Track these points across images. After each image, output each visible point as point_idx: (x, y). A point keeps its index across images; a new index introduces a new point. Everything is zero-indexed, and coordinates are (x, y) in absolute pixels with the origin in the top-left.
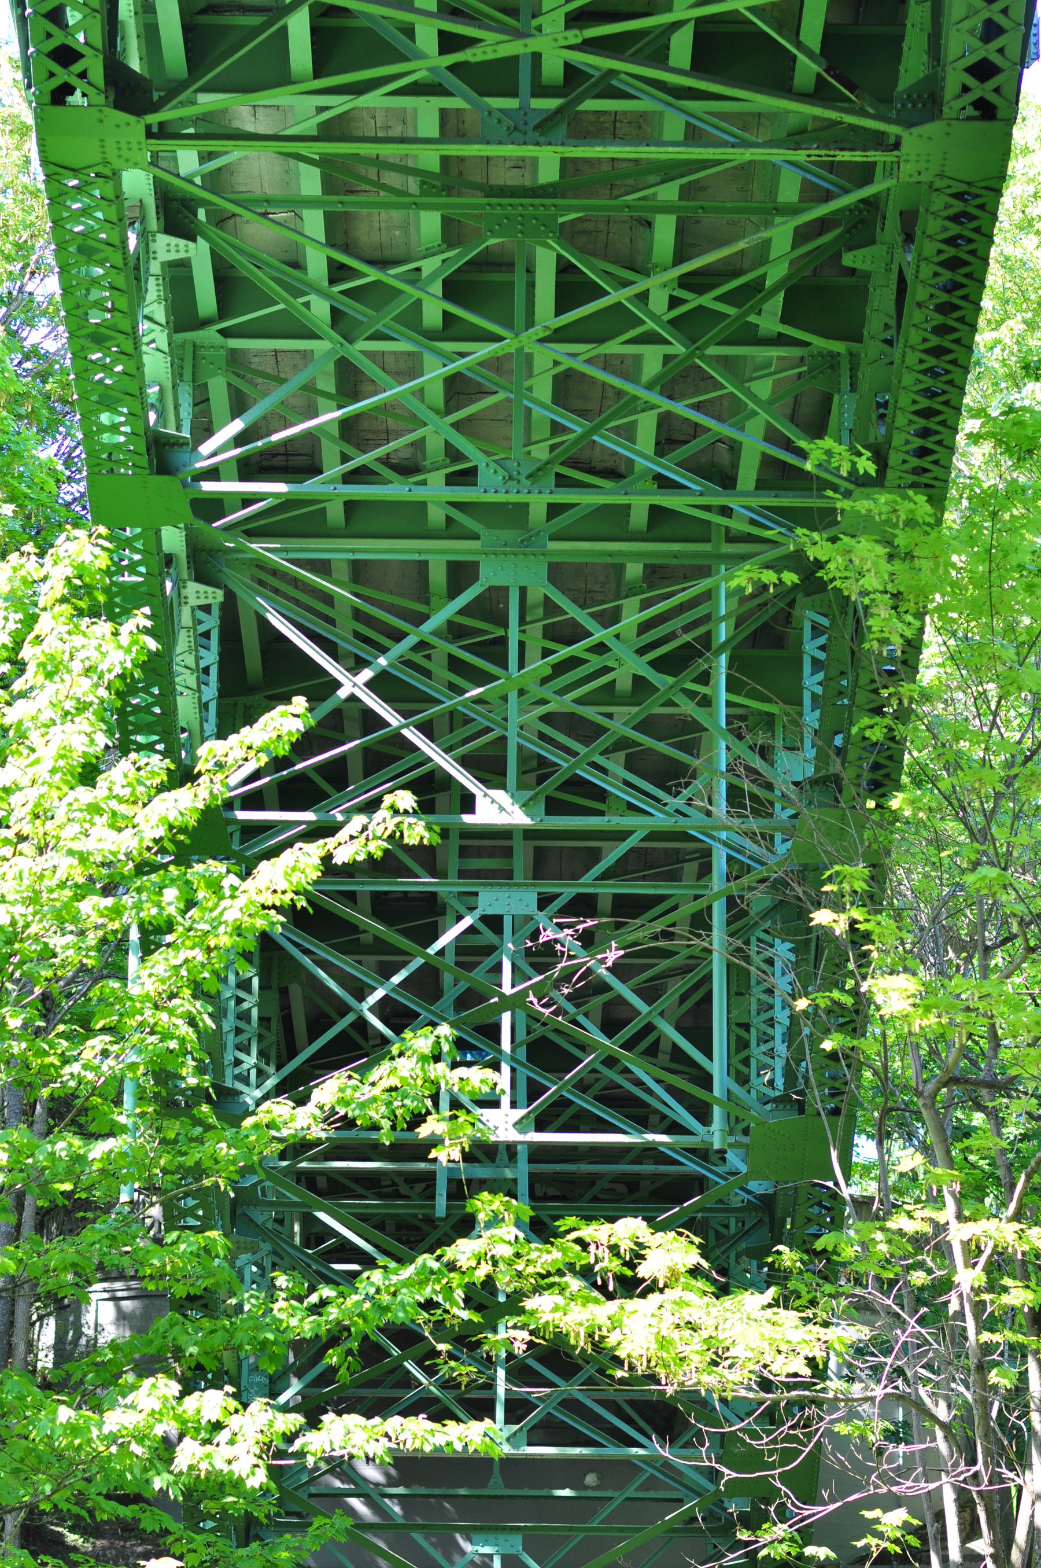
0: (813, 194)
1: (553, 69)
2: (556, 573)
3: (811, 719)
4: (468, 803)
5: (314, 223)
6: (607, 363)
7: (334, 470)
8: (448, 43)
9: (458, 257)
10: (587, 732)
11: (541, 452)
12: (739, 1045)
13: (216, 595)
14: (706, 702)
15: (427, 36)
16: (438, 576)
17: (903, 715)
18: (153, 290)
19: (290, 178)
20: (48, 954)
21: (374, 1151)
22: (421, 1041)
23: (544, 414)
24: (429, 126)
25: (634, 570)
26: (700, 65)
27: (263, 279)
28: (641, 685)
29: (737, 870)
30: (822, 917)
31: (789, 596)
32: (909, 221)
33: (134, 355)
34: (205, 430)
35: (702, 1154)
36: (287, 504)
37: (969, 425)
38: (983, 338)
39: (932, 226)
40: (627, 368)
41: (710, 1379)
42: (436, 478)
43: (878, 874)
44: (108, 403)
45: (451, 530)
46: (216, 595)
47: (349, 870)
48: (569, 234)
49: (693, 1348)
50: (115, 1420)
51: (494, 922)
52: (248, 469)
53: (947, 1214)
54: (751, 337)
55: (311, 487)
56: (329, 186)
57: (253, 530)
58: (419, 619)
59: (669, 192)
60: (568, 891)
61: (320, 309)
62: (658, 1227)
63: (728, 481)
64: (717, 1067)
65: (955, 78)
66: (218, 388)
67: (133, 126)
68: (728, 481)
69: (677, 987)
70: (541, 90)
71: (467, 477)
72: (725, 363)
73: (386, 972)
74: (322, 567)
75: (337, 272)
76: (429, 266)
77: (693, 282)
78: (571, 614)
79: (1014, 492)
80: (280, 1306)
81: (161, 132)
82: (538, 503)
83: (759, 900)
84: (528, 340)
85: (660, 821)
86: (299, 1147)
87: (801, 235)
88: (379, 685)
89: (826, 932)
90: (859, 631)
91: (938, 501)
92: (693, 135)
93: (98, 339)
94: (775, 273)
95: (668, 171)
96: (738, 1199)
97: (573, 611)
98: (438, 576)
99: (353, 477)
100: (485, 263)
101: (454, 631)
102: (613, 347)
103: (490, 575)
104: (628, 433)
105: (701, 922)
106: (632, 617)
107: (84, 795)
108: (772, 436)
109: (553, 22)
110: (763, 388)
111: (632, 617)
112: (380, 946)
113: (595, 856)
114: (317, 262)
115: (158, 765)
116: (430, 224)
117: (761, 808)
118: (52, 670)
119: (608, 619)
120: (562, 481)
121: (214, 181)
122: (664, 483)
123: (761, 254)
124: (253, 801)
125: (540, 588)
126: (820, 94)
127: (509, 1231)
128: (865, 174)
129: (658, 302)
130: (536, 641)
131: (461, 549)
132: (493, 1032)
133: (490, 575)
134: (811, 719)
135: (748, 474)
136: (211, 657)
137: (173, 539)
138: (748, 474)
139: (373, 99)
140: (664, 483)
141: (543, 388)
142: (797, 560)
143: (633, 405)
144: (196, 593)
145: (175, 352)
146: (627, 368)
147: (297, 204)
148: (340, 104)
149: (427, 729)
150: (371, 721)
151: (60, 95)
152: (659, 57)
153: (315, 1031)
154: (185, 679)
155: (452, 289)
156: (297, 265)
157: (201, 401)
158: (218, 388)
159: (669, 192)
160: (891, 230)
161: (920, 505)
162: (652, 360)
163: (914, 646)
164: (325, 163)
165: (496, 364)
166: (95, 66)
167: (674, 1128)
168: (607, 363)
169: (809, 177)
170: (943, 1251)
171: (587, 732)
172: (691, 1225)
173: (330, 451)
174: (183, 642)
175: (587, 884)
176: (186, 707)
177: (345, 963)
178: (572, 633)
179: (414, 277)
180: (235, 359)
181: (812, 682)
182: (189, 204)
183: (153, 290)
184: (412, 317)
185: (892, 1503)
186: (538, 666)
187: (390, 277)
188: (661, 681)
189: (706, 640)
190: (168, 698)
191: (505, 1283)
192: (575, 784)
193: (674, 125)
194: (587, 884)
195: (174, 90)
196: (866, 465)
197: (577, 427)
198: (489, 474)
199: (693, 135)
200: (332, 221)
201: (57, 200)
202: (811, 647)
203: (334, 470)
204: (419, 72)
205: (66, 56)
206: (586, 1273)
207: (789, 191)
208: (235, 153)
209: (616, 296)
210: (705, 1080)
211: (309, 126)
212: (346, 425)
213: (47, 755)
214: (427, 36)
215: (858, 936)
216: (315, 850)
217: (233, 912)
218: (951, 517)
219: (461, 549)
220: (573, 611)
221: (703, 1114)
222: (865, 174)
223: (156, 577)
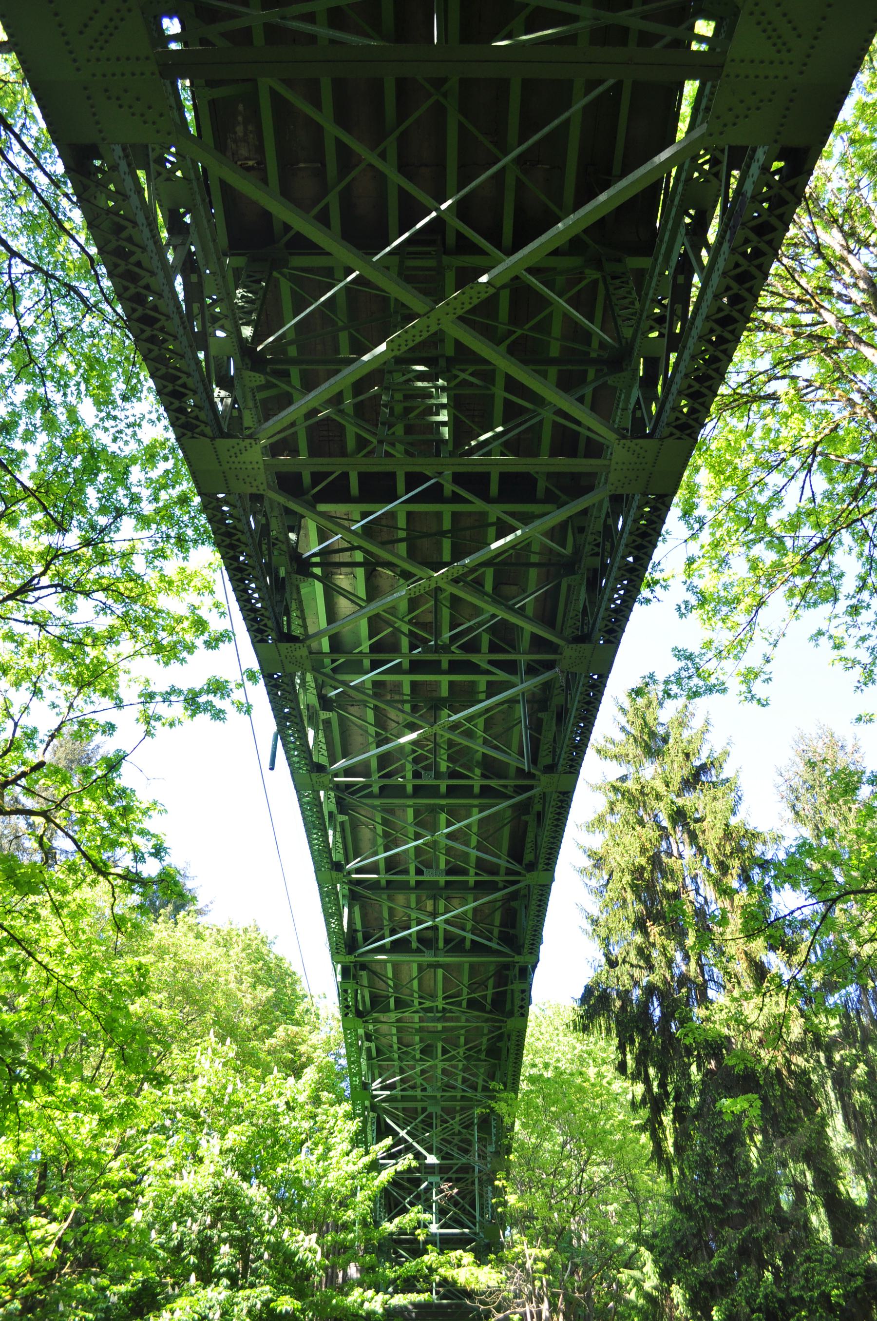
0: (491, 1032)
1: (440, 1007)
2: (443, 1109)
3: (494, 1138)
4: (425, 1158)
5: (395, 1039)
6: (451, 1066)
7: (399, 1088)
8: (420, 1003)
9: (423, 1045)
10: (450, 1143)
11: (439, 1084)
12: (481, 1209)
13: (375, 1115)
14: (473, 1135)
15: (416, 1002)
16: (419, 1110)
17: (511, 1139)
18: (364, 1052)
19: (390, 1030)
20: (339, 1192)
21: (406, 1234)
22: (415, 1209)
23: (440, 1076)
24: (417, 1020)
25: (458, 1108)
26: (468, 1007)
27: (384, 1050)
28: (460, 1133)
29: (480, 1171)
30: (497, 1183)
31: (488, 1115)
32: (509, 1037)
33: (360, 1066)
34: (373, 1080)
35: (475, 1234)
36: (388, 1096)
37: (522, 1078)
38: (524, 1059)
39: (514, 1038)
40: (455, 1067)
41: (477, 1287)
42: (419, 1090)
43: (508, 1174)
44: (355, 1075)
45: (422, 1100)
46: (375, 1115)
47: (401, 1172)
48: (444, 1040)
49: (472, 1279)
50: (350, 1299)
51: (431, 1183)
52: (382, 1089)
53: (525, 1247)
54: (479, 1060)
55: (394, 1092)
56: (398, 1031)
57: (383, 1101)
58: (415, 1119)
59: (463, 1032)
60: (446, 1176)
61: (396, 1056)
62: (465, 1251)
63: (476, 1090)
64: (477, 1214)
65: (516, 1009)
66: (376, 1072)
67: (360, 1021)
68: (476, 1090)
69: (469, 1197)
70: (438, 1012)
71: (424, 1090)
72: (475, 1066)
73: (410, 1194)
74: (396, 1109)
75: (399, 1049)
76: (417, 1047)
77: (469, 1049)
78: (545, 458)
79: (531, 1091)
80: (387, 1271)
81: (366, 1022)
82: (439, 1095)
83: (485, 1178)
84: (437, 1062)
85: (464, 1161)
86: (391, 1234)
87: (488, 1040)
88: (408, 1133)
89: (498, 1187)
90: (502, 1122)
91: (516, 1094)
92: (467, 1021)
93: (353, 1063)
94: (484, 1047)
95: (462, 1028)
96: (483, 1243)
97: (446, 1117)
98: (419, 1110)
99: (402, 1090)
100: (428, 1046)
101: (423, 1121)
102: (453, 1062)
103: (429, 1110)
104: (456, 1080)
105: (473, 1183)
106: (457, 1119)
107: (346, 1158)
108: (484, 1080)
109: (440, 999)
110: (482, 1070)
111: (457, 1119)
112: (408, 1189)
113: (451, 1168)
114: (395, 1047)
115: (362, 1150)
116: (417, 1038)
117: (485, 1158)
118: (340, 1132)
119: (453, 1118)
120: (444, 1090)
121: (376, 1031)
122: (464, 1091)
123: (481, 1044)
124: (383, 1158)
125: (440, 1112)
126: (490, 1012)
127: (435, 1254)
128: (500, 1028)
129: (461, 1053)
130: (439, 1124)
131: (424, 1104)
132: (431, 1207)
133: (429, 1110)
134: (494, 1138)
135: (480, 1088)
136: (375, 1127)
137: (367, 1103)
138: (480, 1088)
139: (406, 1014)
140: (464, 1091)
141: (439, 1071)
142: (489, 1107)
143: (457, 1075)
144: (372, 1114)
145: (368, 1065)
146: (455, 1067)
147: (392, 1035)
148: (400, 1015)
149: (418, 1142)
150: (406, 1141)
151: (346, 1015)
152: (460, 1005)
153: (396, 1207)
154: (369, 1132)
155: (422, 1052)
156: (391, 1047)
157: (373, 1074)
158: (376, 1072)
159: (463, 1032)
160: (506, 1038)
161: (513, 1095)
162: (460, 1067)
163: (513, 1124)
164: (397, 1027)
165: (430, 1067)
166: (353, 1009)
167: (468, 1228)
168: (451, 1066)
169: (304, 367)
170: (524, 1256)
171: (450, 1143)
172: (472, 1250)
173: (398, 1085)
174: (369, 1124)
175: (450, 1175)
176: (369, 1138)
177: (400, 1192)
178: (447, 1122)
179: (414, 1050)
180: (380, 1066)
181: (494, 1131)
182: (371, 1035)
183: (364, 1052)
184: (414, 1057)
185: (515, 1313)
186: (439, 1129)
187: (409, 1049)
188: (464, 1131)
189: (472, 1123)
190: (366, 1137)
191: (434, 1266)
192: (447, 1153)
193: (463, 1019)
194: (450, 1175)
195: (368, 1013)
196: (502, 1087)
197: (446, 1079)
198: (429, 1089)
199: (467, 1021)
200: (398, 1038)
201: (345, 1035)
202: (493, 1123)
203: (399, 1088)
204: (414, 1009)
205: (347, 1007)
206: (449, 1263)
207: (486, 1031)
208: (379, 1026)
209: (453, 1053)
210: (475, 1217)
211: (393, 1020)
212: (401, 1080)
213: (339, 1151)
214: (416, 1002)
215: (504, 1187)
216: (393, 1168)
217: (377, 1182)
218: (520, 1096)
219: (424, 1104)
220: (446, 1117)
221: (475, 1225)
222: (500, 1028)
223: (363, 1112)
